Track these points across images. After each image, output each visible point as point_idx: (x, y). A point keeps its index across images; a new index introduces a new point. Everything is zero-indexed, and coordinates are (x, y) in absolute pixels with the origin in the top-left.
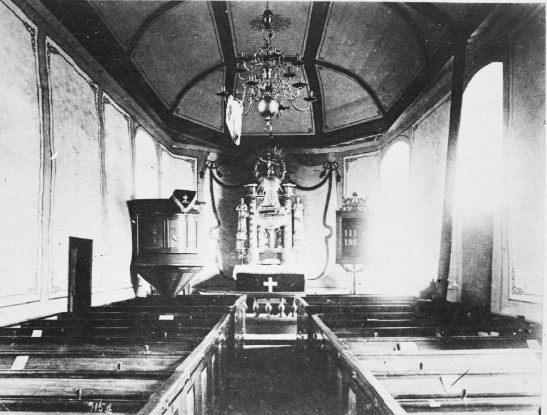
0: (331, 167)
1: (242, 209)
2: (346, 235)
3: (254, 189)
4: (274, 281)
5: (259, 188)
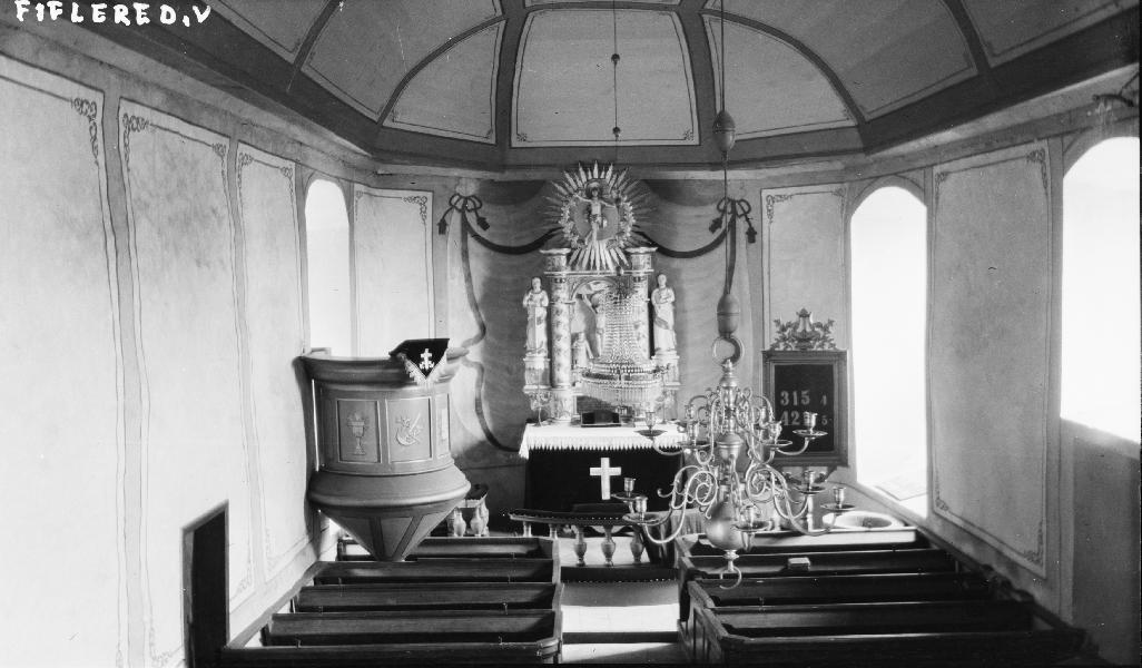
0: (734, 212)
1: (536, 302)
2: (796, 403)
3: (564, 259)
4: (612, 465)
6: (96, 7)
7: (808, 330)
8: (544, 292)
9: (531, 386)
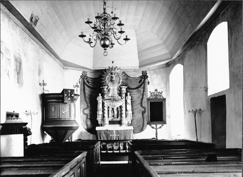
1: (100, 99)
3: (106, 89)
5: (108, 89)
7: (157, 94)
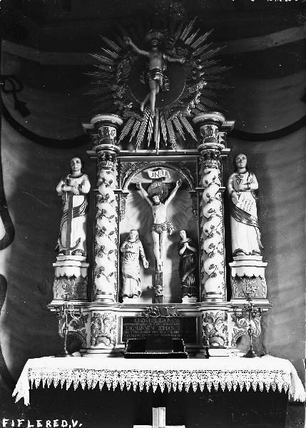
6: (38, 421)
8: (85, 177)
9: (60, 297)
